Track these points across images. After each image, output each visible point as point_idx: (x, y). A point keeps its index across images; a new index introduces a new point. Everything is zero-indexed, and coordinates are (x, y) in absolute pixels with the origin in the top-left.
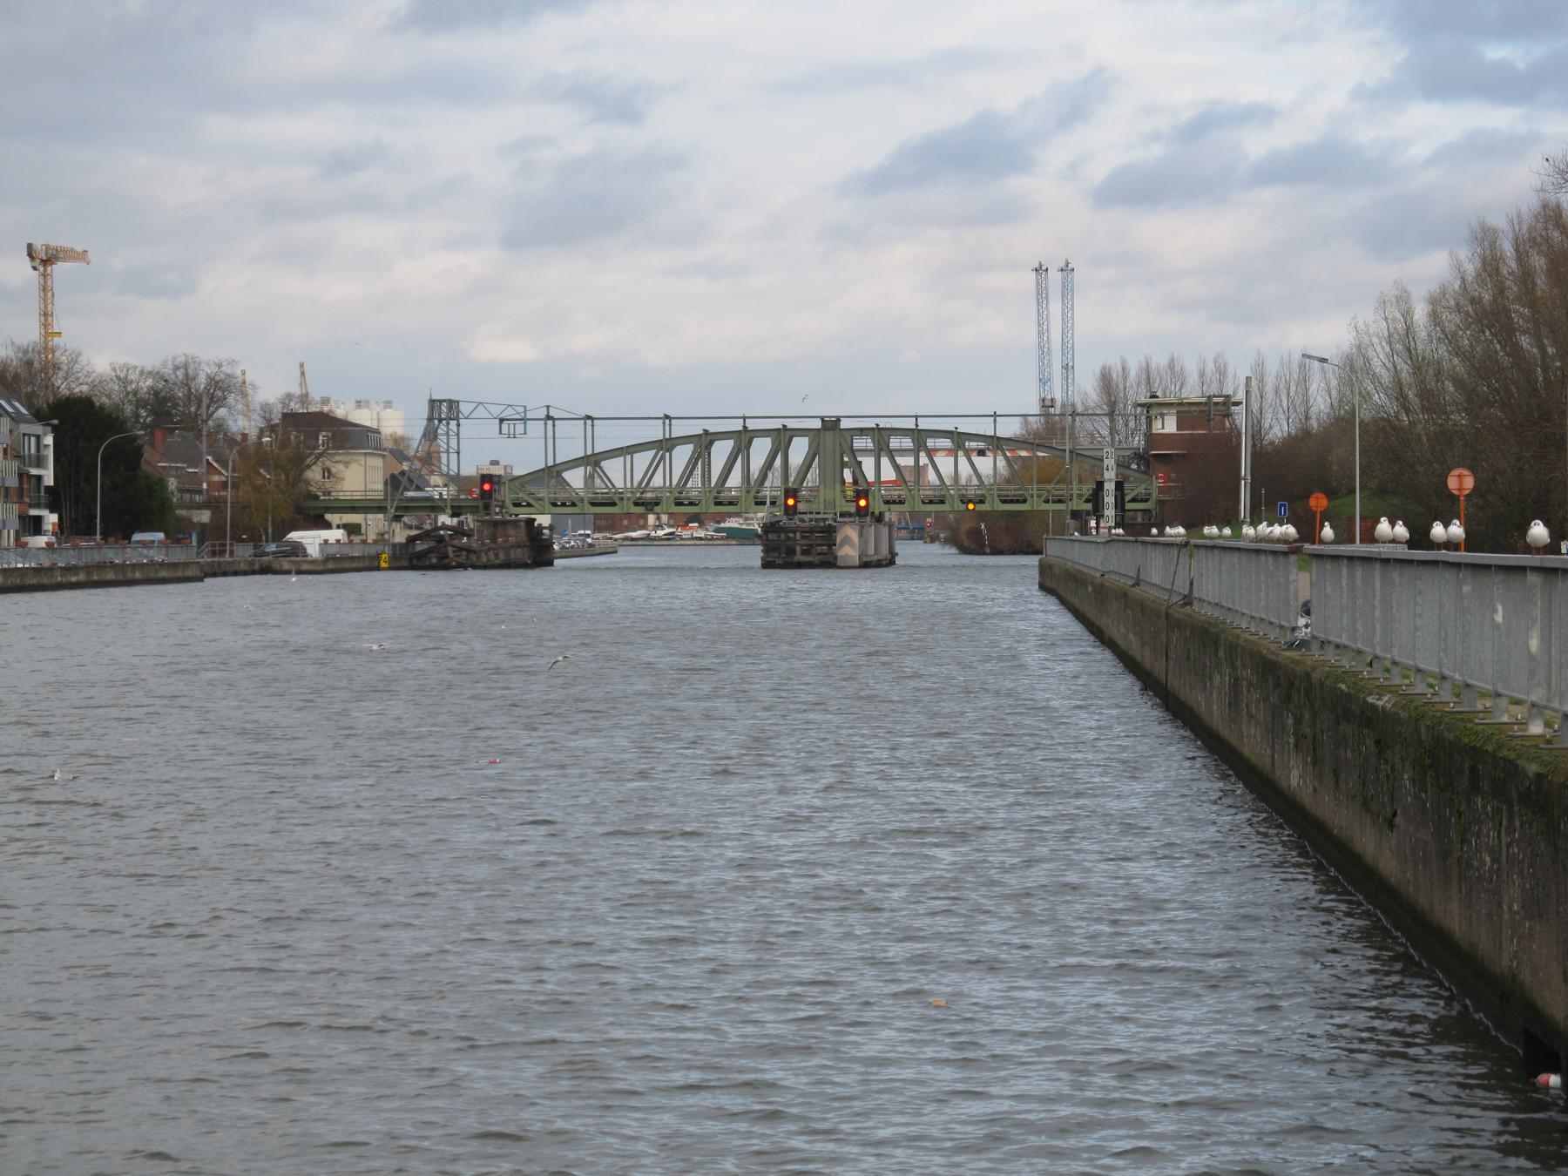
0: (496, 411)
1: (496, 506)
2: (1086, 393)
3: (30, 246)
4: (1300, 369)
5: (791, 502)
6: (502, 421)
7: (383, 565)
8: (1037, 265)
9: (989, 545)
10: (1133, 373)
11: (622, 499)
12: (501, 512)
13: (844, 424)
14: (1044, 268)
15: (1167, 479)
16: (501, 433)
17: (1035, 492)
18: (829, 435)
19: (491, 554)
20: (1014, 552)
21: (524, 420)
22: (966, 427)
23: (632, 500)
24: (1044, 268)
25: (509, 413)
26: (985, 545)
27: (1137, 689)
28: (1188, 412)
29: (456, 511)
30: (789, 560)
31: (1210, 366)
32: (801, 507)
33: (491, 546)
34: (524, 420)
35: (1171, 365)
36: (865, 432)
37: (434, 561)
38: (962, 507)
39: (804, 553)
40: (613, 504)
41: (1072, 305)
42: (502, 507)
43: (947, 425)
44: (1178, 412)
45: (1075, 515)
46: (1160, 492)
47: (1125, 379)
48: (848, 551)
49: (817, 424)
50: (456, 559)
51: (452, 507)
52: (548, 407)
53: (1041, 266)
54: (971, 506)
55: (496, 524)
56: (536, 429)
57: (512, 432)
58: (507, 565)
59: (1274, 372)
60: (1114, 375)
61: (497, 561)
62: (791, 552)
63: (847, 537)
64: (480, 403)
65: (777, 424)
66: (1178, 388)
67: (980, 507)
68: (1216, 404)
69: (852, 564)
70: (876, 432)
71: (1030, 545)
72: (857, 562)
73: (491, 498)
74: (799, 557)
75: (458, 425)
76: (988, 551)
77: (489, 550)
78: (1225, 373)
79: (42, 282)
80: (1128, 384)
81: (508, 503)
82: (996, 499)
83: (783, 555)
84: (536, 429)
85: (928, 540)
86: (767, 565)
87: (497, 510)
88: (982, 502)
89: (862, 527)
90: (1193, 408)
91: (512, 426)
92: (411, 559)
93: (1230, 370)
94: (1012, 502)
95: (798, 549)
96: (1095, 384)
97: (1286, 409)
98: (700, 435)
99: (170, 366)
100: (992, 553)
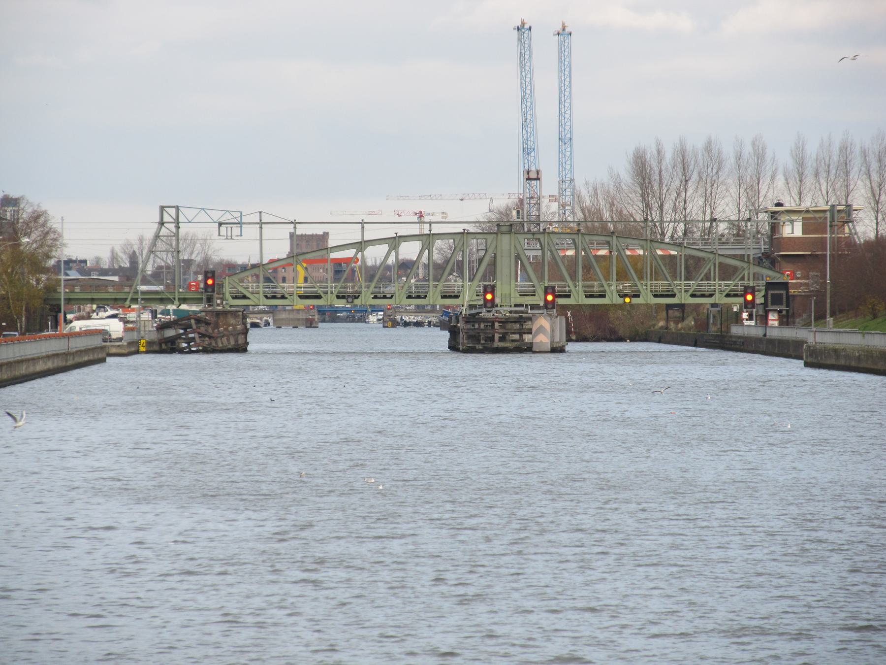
0: (217, 216)
1: (218, 298)
2: (618, 176)
4: (841, 151)
6: (220, 224)
7: (142, 349)
8: (519, 24)
9: (575, 333)
10: (668, 156)
11: (326, 293)
14: (527, 26)
16: (219, 235)
17: (683, 288)
19: (224, 339)
20: (598, 340)
21: (240, 224)
23: (335, 293)
24: (527, 26)
25: (226, 218)
28: (815, 218)
31: (748, 149)
32: (497, 301)
35: (708, 147)
39: (502, 339)
40: (319, 297)
41: (570, 72)
42: (222, 299)
44: (803, 219)
47: (660, 162)
52: (260, 213)
53: (523, 24)
54: (627, 300)
55: (218, 314)
56: (251, 232)
57: (229, 234)
59: (814, 156)
60: (648, 157)
61: (230, 346)
63: (541, 327)
65: (459, 228)
66: (715, 171)
67: (635, 301)
68: (839, 211)
69: (542, 349)
74: (497, 344)
76: (574, 338)
77: (223, 336)
78: (763, 156)
80: (663, 168)
81: (228, 296)
82: (650, 294)
83: (482, 342)
84: (251, 232)
85: (390, 324)
87: (219, 301)
88: (638, 296)
90: (818, 215)
91: (229, 229)
92: (160, 344)
93: (769, 155)
94: (662, 296)
95: (497, 336)
96: (628, 167)
97: (824, 192)
100: (577, 341)
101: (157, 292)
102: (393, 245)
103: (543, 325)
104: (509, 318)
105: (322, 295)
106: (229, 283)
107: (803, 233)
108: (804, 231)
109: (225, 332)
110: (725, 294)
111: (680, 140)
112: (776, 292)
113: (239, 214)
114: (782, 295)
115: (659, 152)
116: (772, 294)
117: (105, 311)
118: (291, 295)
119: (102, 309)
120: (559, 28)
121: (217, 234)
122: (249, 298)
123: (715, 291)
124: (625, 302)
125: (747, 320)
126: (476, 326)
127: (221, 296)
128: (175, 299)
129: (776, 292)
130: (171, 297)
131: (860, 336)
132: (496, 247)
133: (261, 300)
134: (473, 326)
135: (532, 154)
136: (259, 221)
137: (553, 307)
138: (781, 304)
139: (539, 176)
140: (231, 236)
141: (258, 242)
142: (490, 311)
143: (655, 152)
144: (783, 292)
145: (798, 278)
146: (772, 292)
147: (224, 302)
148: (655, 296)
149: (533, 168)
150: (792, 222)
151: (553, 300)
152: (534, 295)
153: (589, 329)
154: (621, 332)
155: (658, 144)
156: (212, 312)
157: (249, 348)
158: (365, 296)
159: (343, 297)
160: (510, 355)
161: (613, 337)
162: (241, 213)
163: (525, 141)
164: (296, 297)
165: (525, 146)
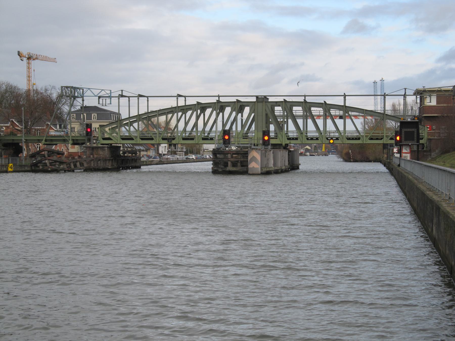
0: (96, 92)
1: (94, 140)
3: (19, 52)
5: (227, 137)
6: (99, 97)
7: (10, 169)
8: (374, 81)
9: (353, 159)
12: (96, 142)
13: (271, 99)
15: (431, 129)
18: (260, 105)
21: (110, 97)
22: (330, 101)
25: (103, 93)
26: (351, 158)
27: (424, 251)
29: (75, 142)
30: (225, 169)
33: (78, 159)
34: (110, 97)
36: (278, 104)
37: (41, 167)
38: (327, 142)
42: (97, 140)
43: (320, 100)
45: (385, 146)
46: (428, 135)
48: (254, 166)
49: (254, 99)
50: (50, 167)
51: (73, 140)
55: (93, 148)
57: (104, 103)
58: (104, 170)
62: (226, 165)
63: (254, 157)
64: (102, 90)
69: (257, 172)
70: (284, 103)
71: (368, 158)
72: (259, 171)
73: (91, 135)
74: (230, 168)
75: (83, 100)
76: (352, 160)
79: (28, 66)
86: (215, 172)
87: (94, 141)
89: (266, 151)
91: (104, 100)
95: (229, 163)
98: (195, 105)
99: (44, 89)
101: (60, 136)
102: (214, 108)
103: (255, 156)
105: (154, 138)
107: (437, 104)
108: (438, 103)
112: (409, 130)
113: (109, 92)
114: (414, 132)
116: (405, 132)
118: (136, 137)
120: (381, 79)
123: (383, 136)
124: (330, 143)
125: (397, 153)
127: (96, 138)
128: (69, 139)
129: (409, 130)
131: (328, 102)
133: (119, 141)
136: (346, 97)
138: (413, 140)
140: (106, 104)
144: (415, 130)
145: (434, 130)
146: (405, 130)
148: (142, 139)
150: (430, 96)
151: (268, 140)
152: (277, 138)
153: (359, 157)
154: (371, 158)
162: (111, 91)
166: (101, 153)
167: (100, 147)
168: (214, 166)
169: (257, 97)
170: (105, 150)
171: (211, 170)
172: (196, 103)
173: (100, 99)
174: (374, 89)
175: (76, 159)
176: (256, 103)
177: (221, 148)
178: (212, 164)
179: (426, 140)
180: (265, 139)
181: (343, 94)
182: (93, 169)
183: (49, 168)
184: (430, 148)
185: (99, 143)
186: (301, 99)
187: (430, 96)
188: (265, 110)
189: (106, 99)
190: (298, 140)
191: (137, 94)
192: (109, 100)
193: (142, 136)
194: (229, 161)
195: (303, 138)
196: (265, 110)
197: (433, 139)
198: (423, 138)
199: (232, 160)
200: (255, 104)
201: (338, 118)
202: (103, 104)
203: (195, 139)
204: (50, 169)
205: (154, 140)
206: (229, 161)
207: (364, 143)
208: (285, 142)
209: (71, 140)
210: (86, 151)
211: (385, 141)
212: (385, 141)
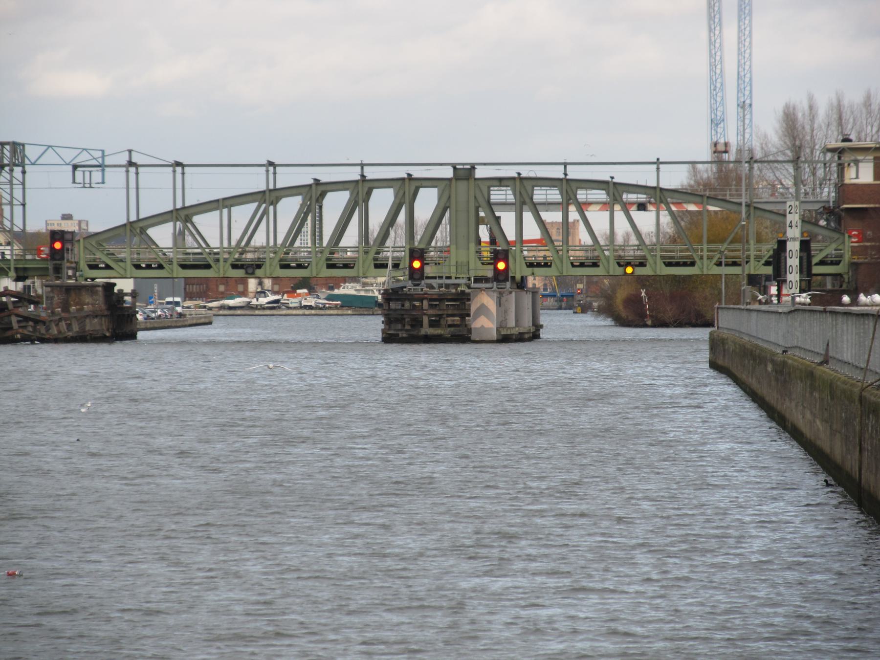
0: (69, 156)
1: (69, 268)
2: (766, 136)
6: (75, 167)
9: (651, 316)
12: (74, 275)
15: (862, 238)
16: (74, 182)
17: (705, 254)
19: (63, 324)
20: (680, 324)
21: (102, 166)
22: (623, 176)
23: (229, 262)
25: (83, 158)
26: (646, 316)
30: (415, 333)
32: (429, 270)
33: (63, 315)
34: (102, 166)
38: (619, 271)
39: (433, 324)
40: (208, 267)
41: (750, 32)
42: (76, 269)
43: (601, 174)
44: (875, 158)
45: (753, 280)
47: (812, 119)
49: (448, 173)
50: (21, 330)
51: (16, 269)
52: (130, 151)
54: (629, 270)
55: (68, 289)
56: (116, 177)
57: (87, 180)
58: (82, 338)
60: (800, 115)
62: (417, 323)
67: (640, 271)
72: (494, 335)
73: (62, 258)
74: (426, 330)
76: (649, 322)
77: (60, 320)
80: (816, 126)
81: (83, 265)
82: (660, 262)
83: (408, 327)
84: (116, 177)
86: (389, 338)
87: (70, 273)
88: (642, 265)
91: (87, 174)
94: (678, 264)
95: (426, 320)
96: (777, 125)
98: (310, 186)
100: (654, 326)
102: (308, 197)
104: (444, 294)
106: (85, 248)
109: (63, 315)
110: (763, 262)
111: (837, 94)
113: (99, 154)
115: (811, 108)
117: (265, 297)
119: (263, 295)
121: (71, 180)
122: (112, 269)
124: (626, 273)
126: (407, 305)
127: (73, 265)
128: (9, 268)
130: (4, 267)
132: (449, 197)
134: (403, 306)
135: (722, 125)
137: (506, 280)
139: (728, 149)
140: (90, 184)
141: (125, 190)
142: (418, 285)
143: (806, 108)
147: (78, 274)
148: (184, 267)
149: (722, 141)
151: (422, 268)
153: (670, 311)
155: (811, 98)
156: (60, 287)
157: (543, 334)
158: (270, 265)
159: (241, 267)
160: (441, 346)
161: (699, 322)
162: (103, 151)
163: (713, 110)
164: (175, 267)
165: (713, 116)
166: (87, 301)
167: (84, 287)
168: (387, 327)
169: (454, 167)
170: (96, 293)
171: (381, 339)
172: (312, 182)
173: (77, 173)
174: (713, 96)
175: (59, 314)
176: (454, 181)
177: (405, 287)
178: (383, 322)
179: (846, 267)
180: (420, 262)
181: (656, 160)
182: (88, 337)
183: (17, 333)
184: (856, 284)
185: (81, 276)
186: (557, 172)
187: (857, 162)
188: (475, 197)
189: (90, 172)
190: (550, 266)
191: (172, 160)
192: (100, 173)
193: (184, 260)
194: (425, 314)
195: (562, 262)
196: (475, 197)
197: (861, 264)
198: (840, 261)
199: (431, 312)
200: (450, 186)
201: (635, 207)
202: (84, 183)
203: (263, 267)
204: (19, 336)
205: (212, 270)
206: (425, 314)
207: (705, 273)
208: (521, 271)
209: (12, 269)
210: (51, 295)
211: (752, 268)
212: (752, 268)
